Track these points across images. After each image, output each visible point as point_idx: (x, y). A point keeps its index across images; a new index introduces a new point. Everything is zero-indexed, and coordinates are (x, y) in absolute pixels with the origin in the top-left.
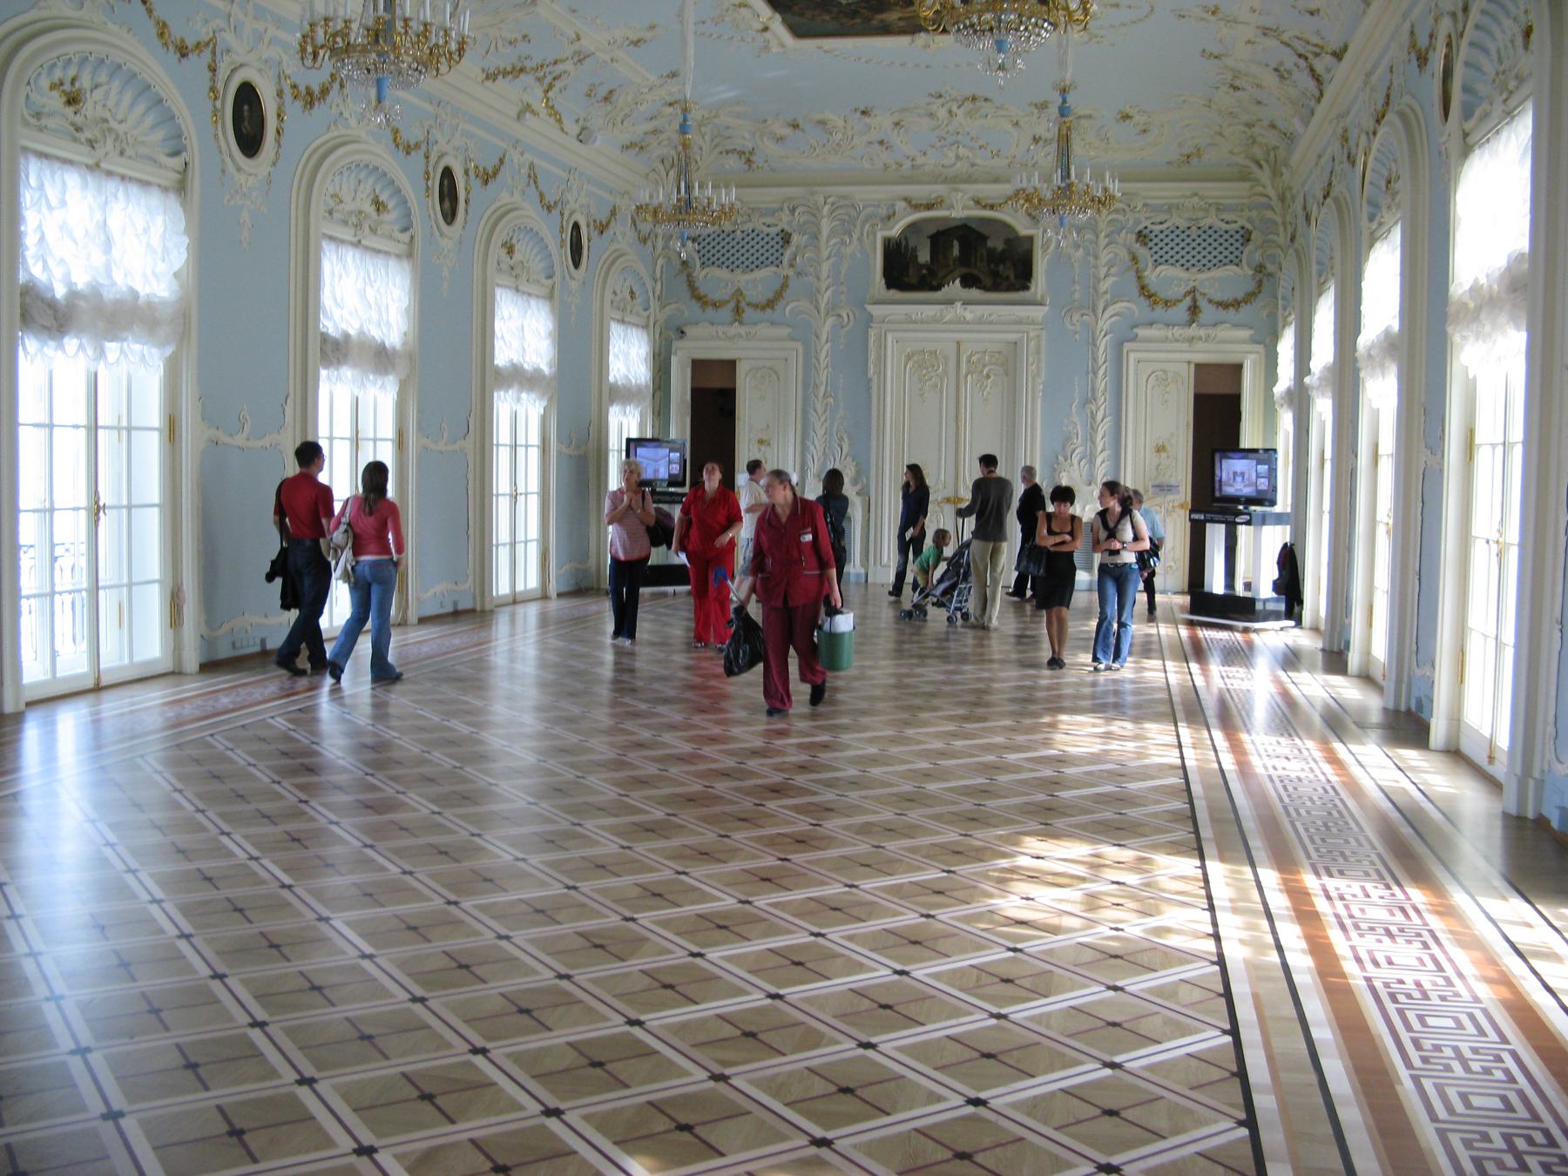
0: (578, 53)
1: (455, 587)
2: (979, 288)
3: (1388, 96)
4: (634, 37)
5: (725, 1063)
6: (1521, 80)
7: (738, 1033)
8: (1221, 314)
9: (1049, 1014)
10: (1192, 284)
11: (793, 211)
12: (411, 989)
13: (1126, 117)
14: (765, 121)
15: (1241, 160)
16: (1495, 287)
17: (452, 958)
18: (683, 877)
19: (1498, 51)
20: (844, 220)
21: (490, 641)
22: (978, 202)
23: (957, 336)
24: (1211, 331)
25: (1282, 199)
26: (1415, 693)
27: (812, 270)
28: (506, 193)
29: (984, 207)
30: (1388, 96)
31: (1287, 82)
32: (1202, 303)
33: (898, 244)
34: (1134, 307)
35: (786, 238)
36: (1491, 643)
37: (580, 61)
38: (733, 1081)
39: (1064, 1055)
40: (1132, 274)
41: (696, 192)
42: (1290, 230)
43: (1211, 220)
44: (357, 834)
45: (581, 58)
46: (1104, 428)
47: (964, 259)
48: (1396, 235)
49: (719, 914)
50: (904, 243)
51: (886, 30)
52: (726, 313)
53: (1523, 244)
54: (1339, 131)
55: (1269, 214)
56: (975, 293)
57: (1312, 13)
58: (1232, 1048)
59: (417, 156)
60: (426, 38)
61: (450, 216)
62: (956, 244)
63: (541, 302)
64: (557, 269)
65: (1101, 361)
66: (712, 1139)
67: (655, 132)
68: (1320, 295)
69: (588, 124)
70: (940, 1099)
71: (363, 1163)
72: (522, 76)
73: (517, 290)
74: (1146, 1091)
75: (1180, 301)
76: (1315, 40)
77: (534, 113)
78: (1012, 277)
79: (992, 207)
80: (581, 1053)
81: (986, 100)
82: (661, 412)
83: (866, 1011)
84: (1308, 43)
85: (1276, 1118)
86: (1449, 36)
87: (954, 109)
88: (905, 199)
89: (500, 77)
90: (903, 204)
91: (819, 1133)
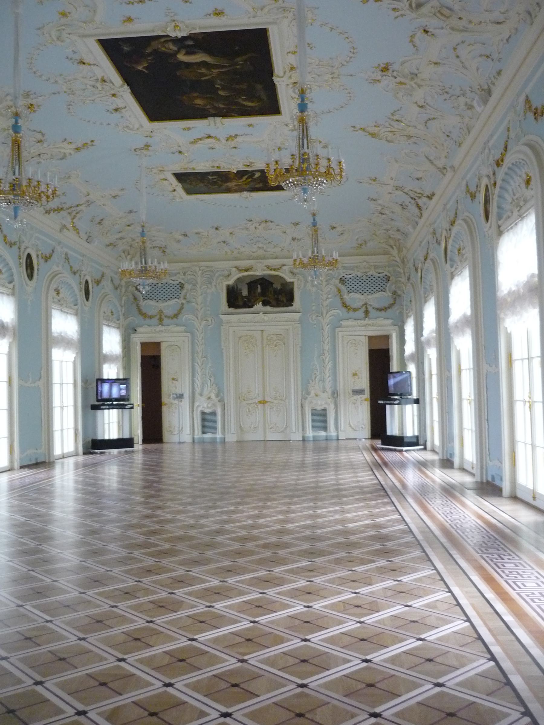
0: (88, 201)
1: (36, 451)
2: (271, 306)
3: (456, 213)
4: (114, 194)
5: (241, 654)
6: (526, 201)
7: (243, 640)
8: (379, 313)
9: (383, 619)
10: (365, 301)
11: (184, 274)
12: (78, 635)
13: (334, 228)
14: (171, 233)
15: (384, 246)
16: (522, 290)
17: (93, 618)
18: (189, 573)
19: (513, 190)
20: (208, 277)
21: (53, 477)
22: (268, 267)
23: (263, 328)
24: (374, 322)
25: (403, 262)
26: (490, 474)
27: (193, 300)
28: (55, 266)
29: (271, 270)
30: (456, 213)
31: (406, 210)
32: (370, 309)
33: (233, 287)
34: (340, 312)
35: (182, 286)
36: (529, 447)
37: (88, 205)
38: (249, 662)
39: (397, 637)
40: (338, 298)
41: (150, 264)
42: (407, 275)
43: (372, 272)
44: (25, 566)
45: (89, 203)
46: (329, 366)
47: (263, 294)
48: (466, 273)
49: (160, 601)
50: (235, 287)
51: (228, 190)
52: (155, 321)
53: (534, 269)
54: (431, 230)
55: (398, 269)
56: (268, 308)
57: (418, 179)
58: (471, 627)
59: (15, 248)
60: (39, 188)
61: (30, 276)
62: (259, 286)
63: (72, 316)
64: (79, 302)
65: (326, 336)
66: (250, 689)
67: (121, 238)
68: (426, 302)
69: (91, 235)
70: (349, 661)
71: (81, 719)
72: (62, 212)
73: (62, 311)
74: (442, 650)
75: (360, 308)
76: (419, 191)
77: (68, 229)
78: (285, 301)
79: (275, 270)
80: (171, 656)
81: (271, 222)
82: (127, 367)
83: (299, 625)
84: (416, 192)
85: (504, 655)
86: (487, 186)
87: (257, 226)
88: (236, 267)
89: (52, 212)
90: (234, 269)
91: (300, 682)
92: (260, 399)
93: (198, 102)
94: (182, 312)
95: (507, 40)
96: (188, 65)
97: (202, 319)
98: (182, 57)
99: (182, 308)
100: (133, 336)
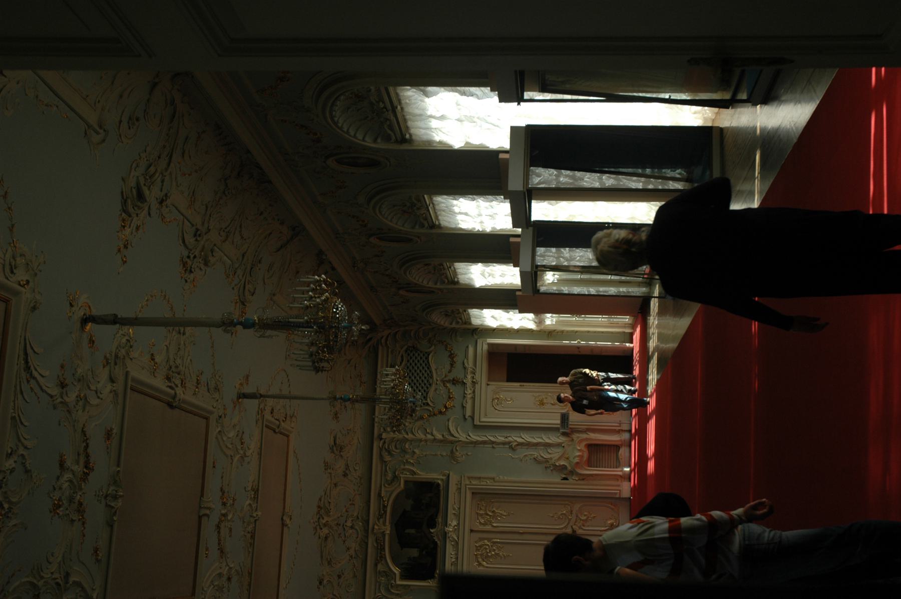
24: (470, 370)
29: (385, 512)
62: (407, 531)
88: (376, 565)
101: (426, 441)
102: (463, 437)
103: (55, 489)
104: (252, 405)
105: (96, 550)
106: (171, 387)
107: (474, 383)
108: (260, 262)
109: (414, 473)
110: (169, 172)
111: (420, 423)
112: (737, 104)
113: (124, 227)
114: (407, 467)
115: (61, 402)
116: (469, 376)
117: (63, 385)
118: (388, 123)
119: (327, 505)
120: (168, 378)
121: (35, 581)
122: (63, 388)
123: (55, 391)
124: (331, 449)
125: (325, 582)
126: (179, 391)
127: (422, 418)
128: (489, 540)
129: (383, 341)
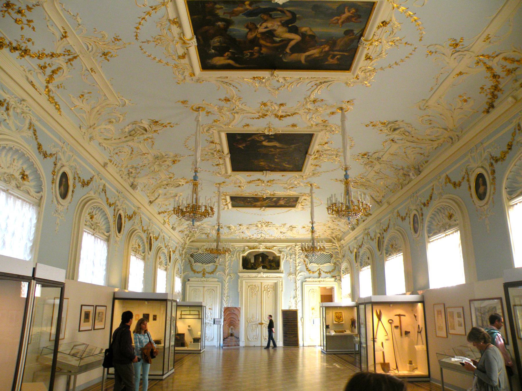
24: (324, 279)
29: (268, 249)
32: (322, 272)
47: (263, 261)
51: (255, 206)
52: (201, 275)
56: (266, 270)
62: (260, 258)
88: (248, 246)
92: (260, 322)
93: (262, 163)
94: (216, 270)
95: (435, 149)
96: (266, 147)
97: (227, 275)
98: (265, 143)
99: (216, 268)
100: (187, 283)
101: (296, 263)
102: (298, 277)
103: (271, 103)
104: (308, 190)
105: (248, 125)
106: (314, 153)
107: (320, 281)
108: (366, 189)
109: (283, 259)
110: (406, 142)
111: (302, 260)
112: (300, 368)
113: (382, 124)
114: (285, 256)
115: (307, 101)
116: (322, 280)
117: (314, 101)
118: (438, 232)
119: (269, 226)
120: (318, 151)
121: (234, 98)
122: (313, 101)
123: (312, 97)
124: (291, 226)
125: (240, 227)
126: (313, 157)
127: (305, 261)
128: (258, 290)
129: (334, 244)
